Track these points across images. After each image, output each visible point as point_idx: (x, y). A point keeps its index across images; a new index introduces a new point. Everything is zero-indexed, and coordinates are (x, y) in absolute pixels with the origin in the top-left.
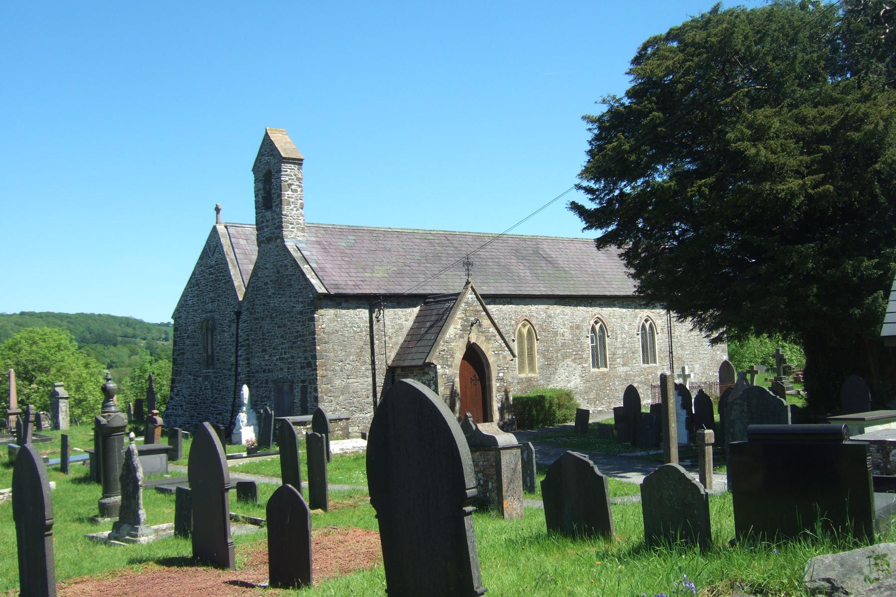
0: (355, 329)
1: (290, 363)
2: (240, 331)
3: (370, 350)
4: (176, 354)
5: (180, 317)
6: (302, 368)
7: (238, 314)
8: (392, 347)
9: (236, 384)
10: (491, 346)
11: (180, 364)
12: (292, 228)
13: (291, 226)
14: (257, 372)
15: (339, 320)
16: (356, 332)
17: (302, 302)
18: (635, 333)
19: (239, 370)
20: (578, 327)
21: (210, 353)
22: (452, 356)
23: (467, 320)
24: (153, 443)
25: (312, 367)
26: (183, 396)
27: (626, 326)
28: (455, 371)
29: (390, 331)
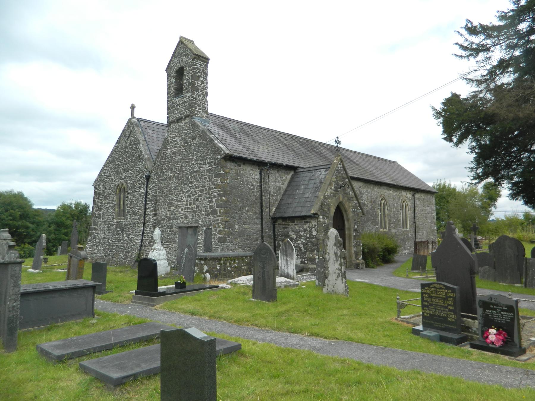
0: (250, 186)
1: (195, 212)
2: (148, 190)
3: (259, 204)
4: (94, 210)
5: (99, 185)
6: (207, 215)
7: (148, 178)
8: (273, 203)
9: (144, 229)
10: (351, 204)
11: (97, 217)
12: (199, 109)
13: (198, 108)
14: (163, 219)
15: (239, 178)
16: (250, 189)
17: (209, 163)
18: (399, 209)
19: (147, 218)
20: (374, 202)
21: (122, 208)
22: (329, 210)
23: (337, 184)
24: (81, 278)
25: (217, 214)
26: (99, 239)
27: (395, 204)
28: (331, 222)
29: (272, 191)
